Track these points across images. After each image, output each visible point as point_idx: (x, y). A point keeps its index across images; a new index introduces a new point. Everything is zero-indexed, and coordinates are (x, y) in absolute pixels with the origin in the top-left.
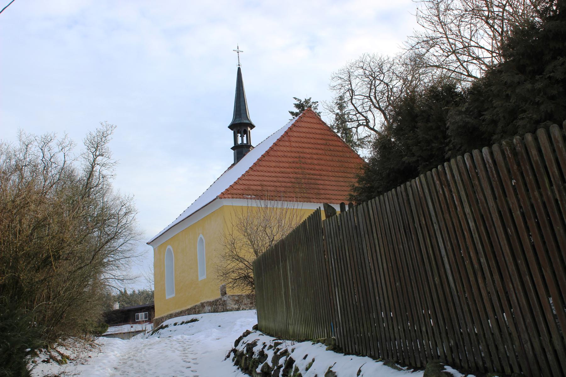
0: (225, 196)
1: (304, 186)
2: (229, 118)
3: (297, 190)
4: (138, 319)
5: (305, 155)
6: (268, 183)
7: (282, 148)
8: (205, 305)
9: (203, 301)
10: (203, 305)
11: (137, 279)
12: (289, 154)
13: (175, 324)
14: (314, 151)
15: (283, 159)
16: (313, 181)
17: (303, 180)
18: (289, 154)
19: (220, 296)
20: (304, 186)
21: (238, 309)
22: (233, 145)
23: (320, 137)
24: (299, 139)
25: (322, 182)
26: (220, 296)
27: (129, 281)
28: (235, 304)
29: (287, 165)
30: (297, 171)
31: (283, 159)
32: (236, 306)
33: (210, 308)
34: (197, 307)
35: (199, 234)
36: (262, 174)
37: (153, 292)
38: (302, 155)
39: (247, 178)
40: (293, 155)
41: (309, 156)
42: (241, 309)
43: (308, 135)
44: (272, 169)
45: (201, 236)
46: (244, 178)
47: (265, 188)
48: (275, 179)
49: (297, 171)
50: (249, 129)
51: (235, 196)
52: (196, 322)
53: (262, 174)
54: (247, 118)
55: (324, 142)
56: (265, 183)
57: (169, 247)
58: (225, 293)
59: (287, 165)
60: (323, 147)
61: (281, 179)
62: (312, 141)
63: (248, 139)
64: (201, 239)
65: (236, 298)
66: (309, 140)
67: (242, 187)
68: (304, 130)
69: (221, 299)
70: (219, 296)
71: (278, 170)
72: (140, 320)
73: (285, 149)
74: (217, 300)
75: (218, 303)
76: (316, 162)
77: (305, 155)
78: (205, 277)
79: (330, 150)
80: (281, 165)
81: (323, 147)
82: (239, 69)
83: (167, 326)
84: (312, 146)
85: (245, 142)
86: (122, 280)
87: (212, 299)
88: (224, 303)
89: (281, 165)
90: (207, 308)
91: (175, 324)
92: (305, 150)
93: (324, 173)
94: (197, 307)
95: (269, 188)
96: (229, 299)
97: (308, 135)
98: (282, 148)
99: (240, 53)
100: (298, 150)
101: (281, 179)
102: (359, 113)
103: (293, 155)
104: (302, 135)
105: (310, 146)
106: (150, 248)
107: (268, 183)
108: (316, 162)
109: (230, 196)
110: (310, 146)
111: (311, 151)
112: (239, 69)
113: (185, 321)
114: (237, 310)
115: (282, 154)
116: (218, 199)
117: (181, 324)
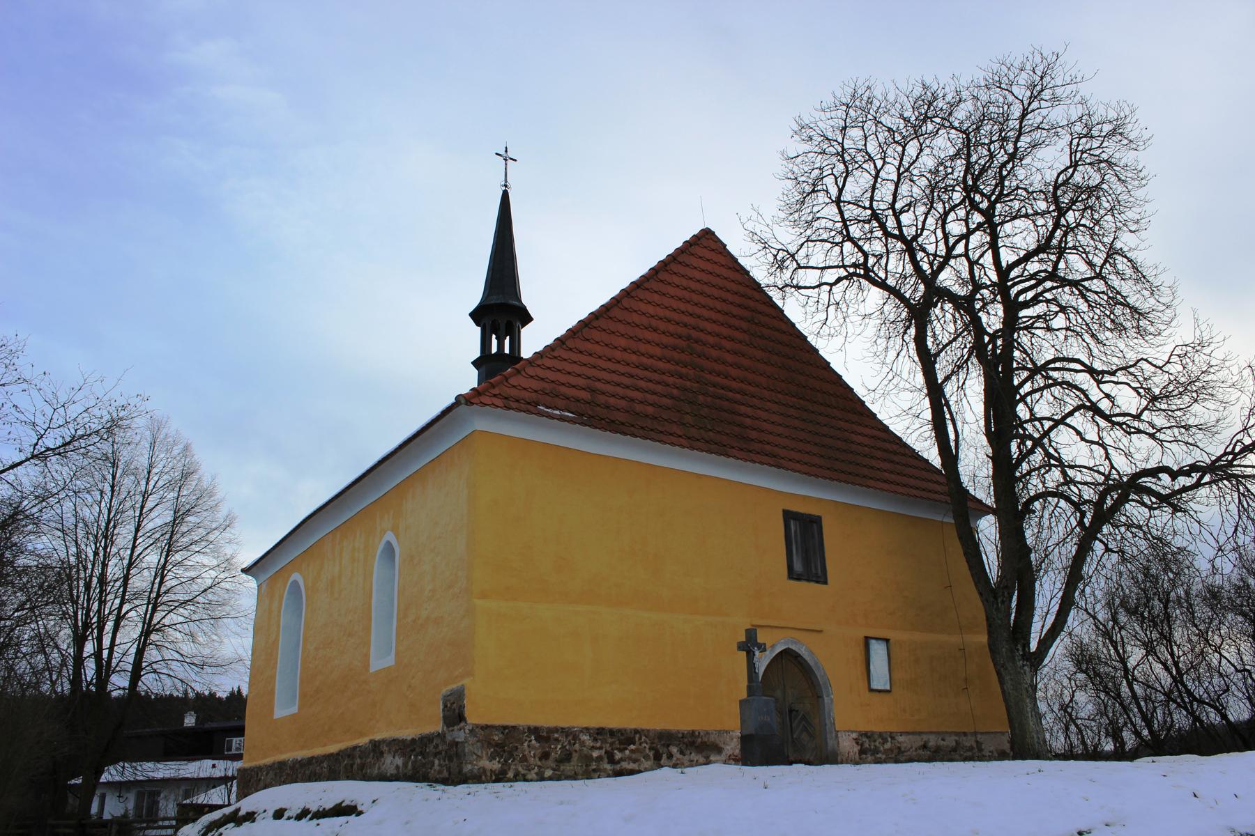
0: (485, 399)
1: (705, 411)
2: (475, 296)
3: (688, 419)
4: (230, 749)
5: (703, 336)
6: (609, 388)
7: (643, 307)
8: (385, 748)
9: (378, 737)
10: (377, 748)
11: (232, 666)
12: (662, 326)
13: (279, 814)
14: (725, 331)
15: (648, 335)
16: (726, 405)
17: (701, 398)
18: (662, 326)
19: (439, 727)
20: (705, 411)
21: (500, 777)
22: (477, 354)
23: (738, 300)
24: (709, 267)
25: (749, 411)
26: (439, 727)
27: (214, 669)
28: (492, 758)
29: (658, 351)
30: (684, 371)
31: (648, 335)
32: (496, 765)
33: (399, 761)
34: (357, 753)
35: (384, 532)
36: (592, 360)
37: (236, 700)
38: (694, 334)
39: (549, 363)
40: (672, 328)
41: (711, 340)
42: (510, 775)
43: (707, 289)
44: (618, 355)
45: (390, 536)
46: (539, 362)
47: (602, 399)
48: (627, 381)
49: (684, 371)
50: (518, 324)
51: (514, 405)
52: (352, 818)
53: (592, 360)
54: (517, 296)
55: (746, 314)
56: (599, 385)
57: (296, 576)
58: (461, 718)
59: (658, 351)
60: (744, 325)
61: (642, 384)
62: (719, 305)
63: (516, 344)
64: (389, 548)
65: (496, 737)
66: (711, 303)
67: (535, 384)
68: (698, 275)
69: (441, 736)
70: (434, 725)
71: (634, 358)
72: (234, 752)
73: (651, 310)
74: (426, 740)
75: (430, 749)
76: (730, 358)
77: (703, 336)
78: (390, 661)
79: (762, 337)
80: (643, 348)
81: (744, 325)
82: (505, 196)
83: (251, 817)
84: (721, 318)
85: (507, 351)
86: (202, 666)
87: (408, 733)
88: (454, 752)
89: (643, 348)
90: (392, 762)
91: (279, 814)
92: (703, 324)
93: (752, 389)
94: (357, 753)
95: (612, 401)
96: (472, 740)
97: (707, 289)
98: (643, 307)
99: (509, 162)
100: (686, 319)
101: (642, 384)
102: (851, 239)
103: (672, 328)
104: (693, 285)
105: (713, 315)
106: (251, 583)
107: (609, 388)
108: (730, 358)
109: (497, 401)
110: (713, 315)
111: (716, 328)
112: (505, 196)
113: (314, 809)
114: (497, 781)
115: (645, 321)
116: (463, 408)
117: (299, 817)
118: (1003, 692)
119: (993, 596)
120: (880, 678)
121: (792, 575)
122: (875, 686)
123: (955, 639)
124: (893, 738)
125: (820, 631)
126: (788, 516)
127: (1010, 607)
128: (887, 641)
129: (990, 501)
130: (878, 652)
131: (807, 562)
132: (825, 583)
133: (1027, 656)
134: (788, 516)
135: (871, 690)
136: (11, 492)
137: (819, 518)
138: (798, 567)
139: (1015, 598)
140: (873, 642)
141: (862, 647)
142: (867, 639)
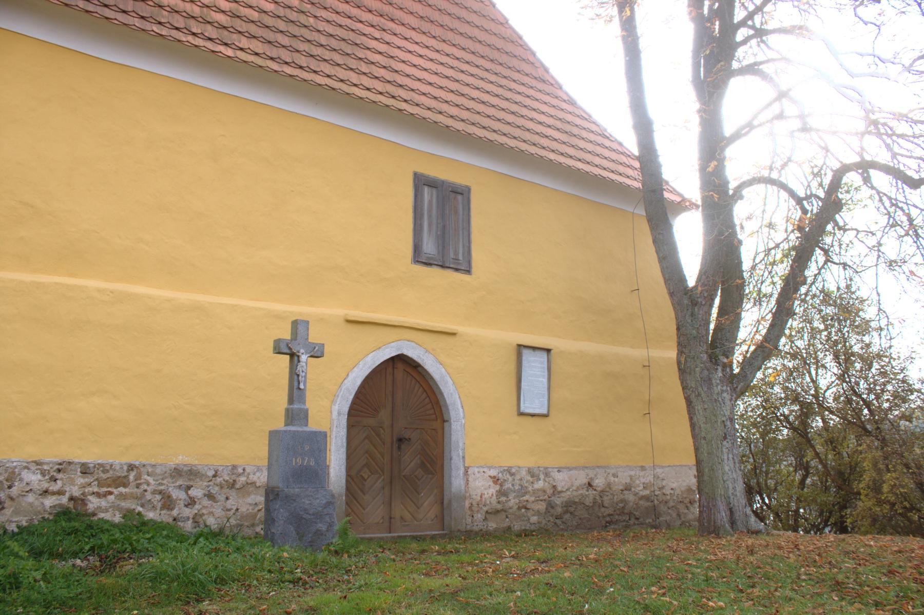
89: (382, 48)
118: (693, 426)
119: (689, 303)
120: (534, 403)
121: (419, 257)
122: (526, 407)
123: (639, 353)
124: (547, 475)
125: (454, 334)
126: (421, 182)
127: (708, 329)
128: (548, 351)
129: (699, 203)
130: (534, 365)
131: (442, 240)
132: (468, 272)
133: (731, 379)
134: (421, 182)
135: (521, 414)
136: (835, 289)
137: (468, 189)
138: (429, 247)
139: (712, 326)
140: (526, 353)
141: (514, 357)
142: (519, 346)
